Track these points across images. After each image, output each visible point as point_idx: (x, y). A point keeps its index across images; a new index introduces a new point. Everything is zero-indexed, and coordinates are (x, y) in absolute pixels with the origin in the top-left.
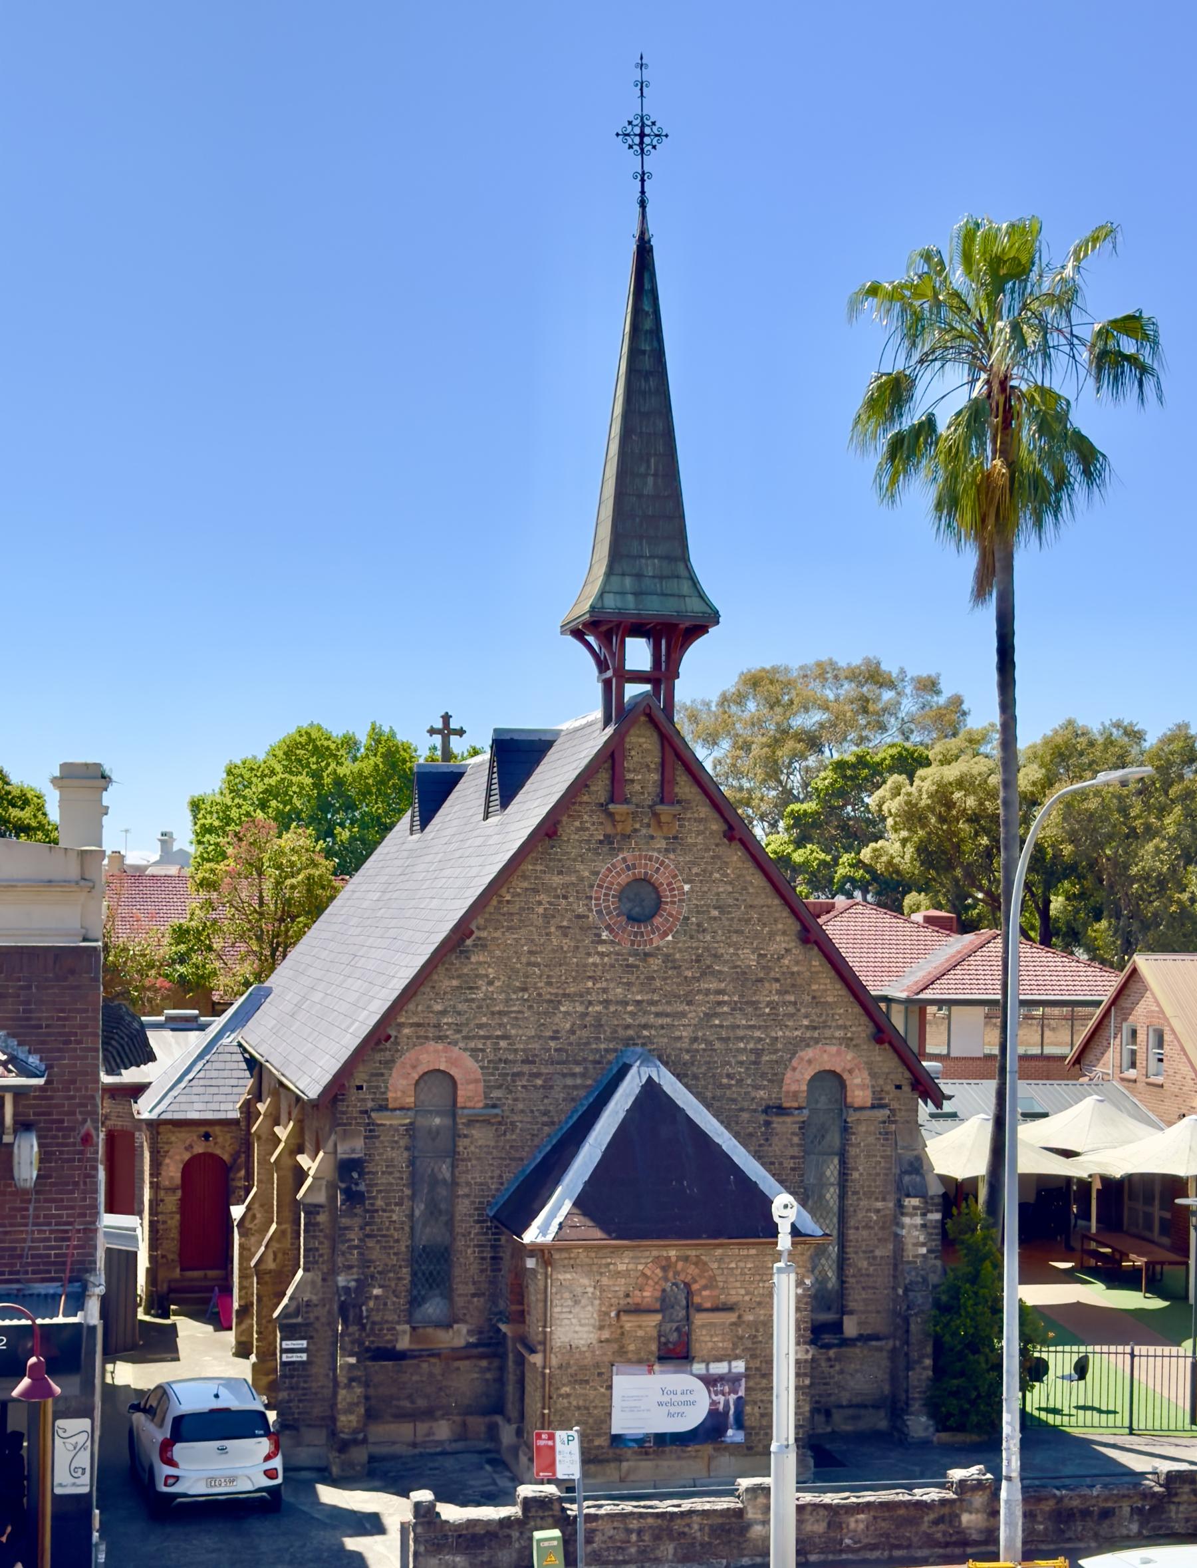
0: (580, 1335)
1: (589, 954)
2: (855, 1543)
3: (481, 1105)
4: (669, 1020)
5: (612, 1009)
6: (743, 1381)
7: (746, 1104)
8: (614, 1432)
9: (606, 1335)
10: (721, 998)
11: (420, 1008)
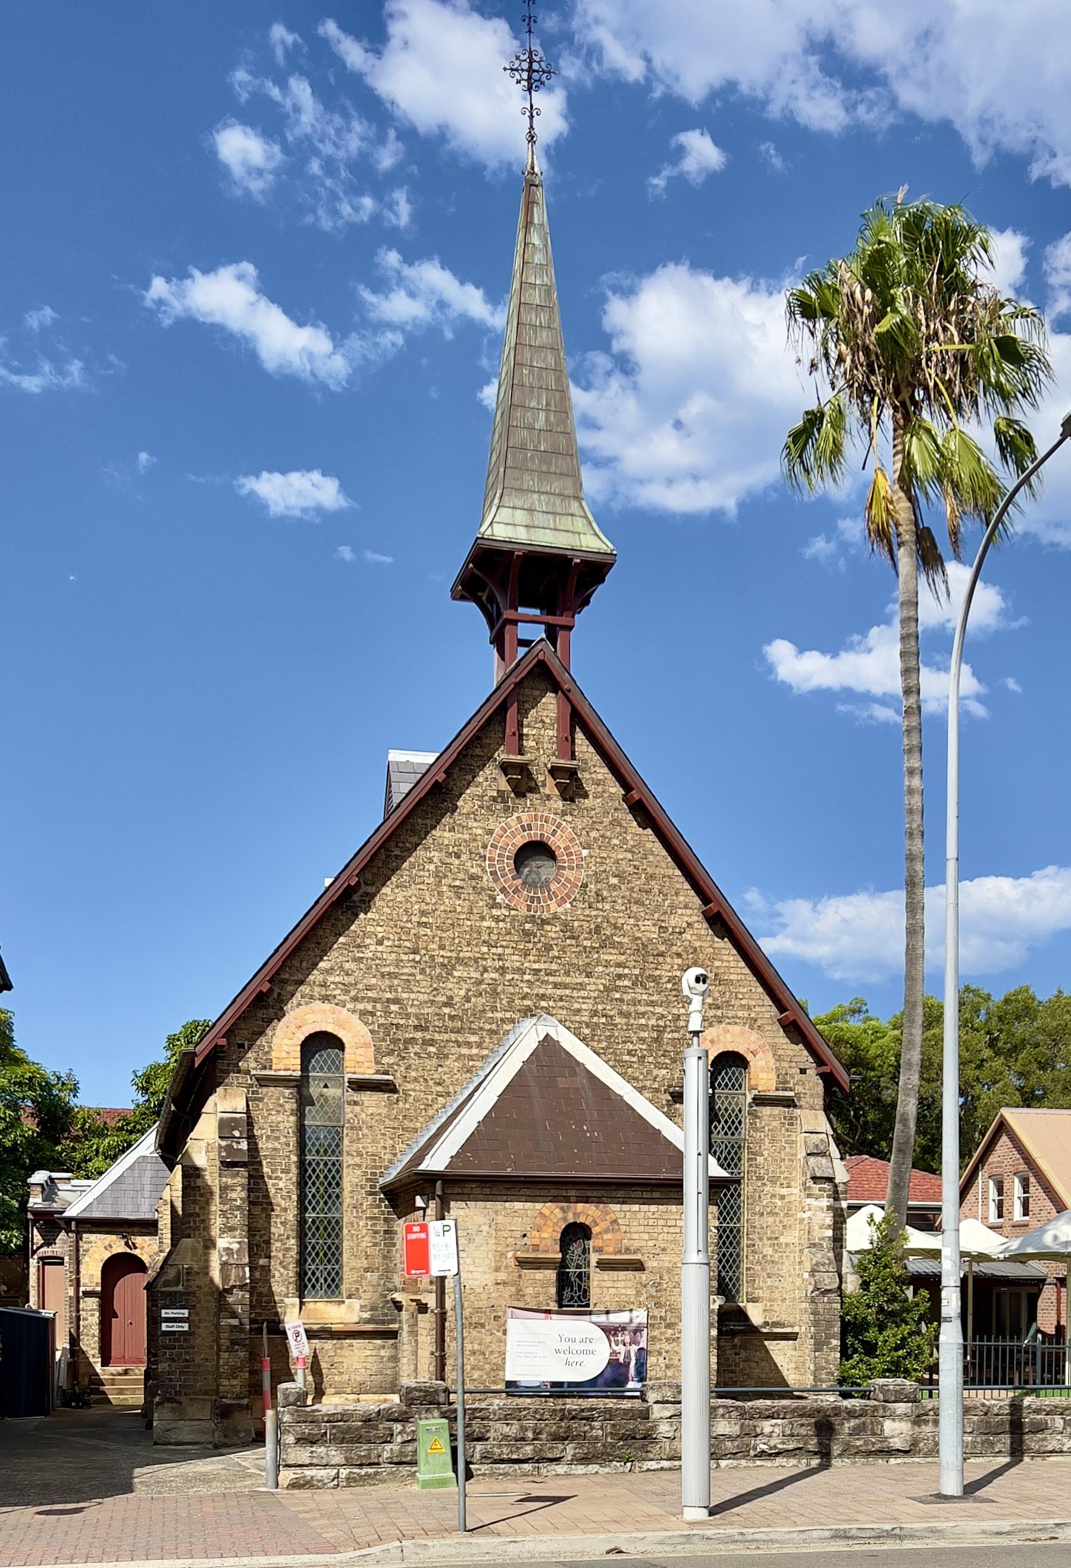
0: (476, 1275)
1: (483, 918)
2: (771, 1448)
3: (372, 1071)
4: (567, 992)
5: (508, 977)
6: (645, 1333)
7: (648, 1083)
8: (507, 1379)
9: (502, 1276)
10: (620, 971)
11: (304, 964)
